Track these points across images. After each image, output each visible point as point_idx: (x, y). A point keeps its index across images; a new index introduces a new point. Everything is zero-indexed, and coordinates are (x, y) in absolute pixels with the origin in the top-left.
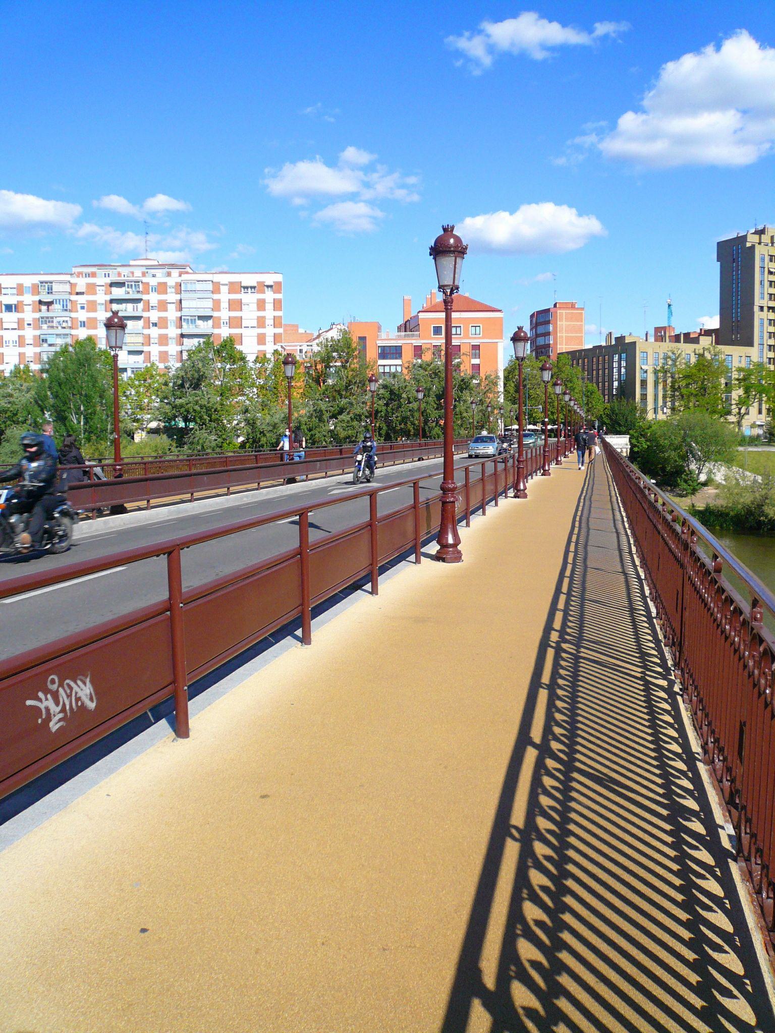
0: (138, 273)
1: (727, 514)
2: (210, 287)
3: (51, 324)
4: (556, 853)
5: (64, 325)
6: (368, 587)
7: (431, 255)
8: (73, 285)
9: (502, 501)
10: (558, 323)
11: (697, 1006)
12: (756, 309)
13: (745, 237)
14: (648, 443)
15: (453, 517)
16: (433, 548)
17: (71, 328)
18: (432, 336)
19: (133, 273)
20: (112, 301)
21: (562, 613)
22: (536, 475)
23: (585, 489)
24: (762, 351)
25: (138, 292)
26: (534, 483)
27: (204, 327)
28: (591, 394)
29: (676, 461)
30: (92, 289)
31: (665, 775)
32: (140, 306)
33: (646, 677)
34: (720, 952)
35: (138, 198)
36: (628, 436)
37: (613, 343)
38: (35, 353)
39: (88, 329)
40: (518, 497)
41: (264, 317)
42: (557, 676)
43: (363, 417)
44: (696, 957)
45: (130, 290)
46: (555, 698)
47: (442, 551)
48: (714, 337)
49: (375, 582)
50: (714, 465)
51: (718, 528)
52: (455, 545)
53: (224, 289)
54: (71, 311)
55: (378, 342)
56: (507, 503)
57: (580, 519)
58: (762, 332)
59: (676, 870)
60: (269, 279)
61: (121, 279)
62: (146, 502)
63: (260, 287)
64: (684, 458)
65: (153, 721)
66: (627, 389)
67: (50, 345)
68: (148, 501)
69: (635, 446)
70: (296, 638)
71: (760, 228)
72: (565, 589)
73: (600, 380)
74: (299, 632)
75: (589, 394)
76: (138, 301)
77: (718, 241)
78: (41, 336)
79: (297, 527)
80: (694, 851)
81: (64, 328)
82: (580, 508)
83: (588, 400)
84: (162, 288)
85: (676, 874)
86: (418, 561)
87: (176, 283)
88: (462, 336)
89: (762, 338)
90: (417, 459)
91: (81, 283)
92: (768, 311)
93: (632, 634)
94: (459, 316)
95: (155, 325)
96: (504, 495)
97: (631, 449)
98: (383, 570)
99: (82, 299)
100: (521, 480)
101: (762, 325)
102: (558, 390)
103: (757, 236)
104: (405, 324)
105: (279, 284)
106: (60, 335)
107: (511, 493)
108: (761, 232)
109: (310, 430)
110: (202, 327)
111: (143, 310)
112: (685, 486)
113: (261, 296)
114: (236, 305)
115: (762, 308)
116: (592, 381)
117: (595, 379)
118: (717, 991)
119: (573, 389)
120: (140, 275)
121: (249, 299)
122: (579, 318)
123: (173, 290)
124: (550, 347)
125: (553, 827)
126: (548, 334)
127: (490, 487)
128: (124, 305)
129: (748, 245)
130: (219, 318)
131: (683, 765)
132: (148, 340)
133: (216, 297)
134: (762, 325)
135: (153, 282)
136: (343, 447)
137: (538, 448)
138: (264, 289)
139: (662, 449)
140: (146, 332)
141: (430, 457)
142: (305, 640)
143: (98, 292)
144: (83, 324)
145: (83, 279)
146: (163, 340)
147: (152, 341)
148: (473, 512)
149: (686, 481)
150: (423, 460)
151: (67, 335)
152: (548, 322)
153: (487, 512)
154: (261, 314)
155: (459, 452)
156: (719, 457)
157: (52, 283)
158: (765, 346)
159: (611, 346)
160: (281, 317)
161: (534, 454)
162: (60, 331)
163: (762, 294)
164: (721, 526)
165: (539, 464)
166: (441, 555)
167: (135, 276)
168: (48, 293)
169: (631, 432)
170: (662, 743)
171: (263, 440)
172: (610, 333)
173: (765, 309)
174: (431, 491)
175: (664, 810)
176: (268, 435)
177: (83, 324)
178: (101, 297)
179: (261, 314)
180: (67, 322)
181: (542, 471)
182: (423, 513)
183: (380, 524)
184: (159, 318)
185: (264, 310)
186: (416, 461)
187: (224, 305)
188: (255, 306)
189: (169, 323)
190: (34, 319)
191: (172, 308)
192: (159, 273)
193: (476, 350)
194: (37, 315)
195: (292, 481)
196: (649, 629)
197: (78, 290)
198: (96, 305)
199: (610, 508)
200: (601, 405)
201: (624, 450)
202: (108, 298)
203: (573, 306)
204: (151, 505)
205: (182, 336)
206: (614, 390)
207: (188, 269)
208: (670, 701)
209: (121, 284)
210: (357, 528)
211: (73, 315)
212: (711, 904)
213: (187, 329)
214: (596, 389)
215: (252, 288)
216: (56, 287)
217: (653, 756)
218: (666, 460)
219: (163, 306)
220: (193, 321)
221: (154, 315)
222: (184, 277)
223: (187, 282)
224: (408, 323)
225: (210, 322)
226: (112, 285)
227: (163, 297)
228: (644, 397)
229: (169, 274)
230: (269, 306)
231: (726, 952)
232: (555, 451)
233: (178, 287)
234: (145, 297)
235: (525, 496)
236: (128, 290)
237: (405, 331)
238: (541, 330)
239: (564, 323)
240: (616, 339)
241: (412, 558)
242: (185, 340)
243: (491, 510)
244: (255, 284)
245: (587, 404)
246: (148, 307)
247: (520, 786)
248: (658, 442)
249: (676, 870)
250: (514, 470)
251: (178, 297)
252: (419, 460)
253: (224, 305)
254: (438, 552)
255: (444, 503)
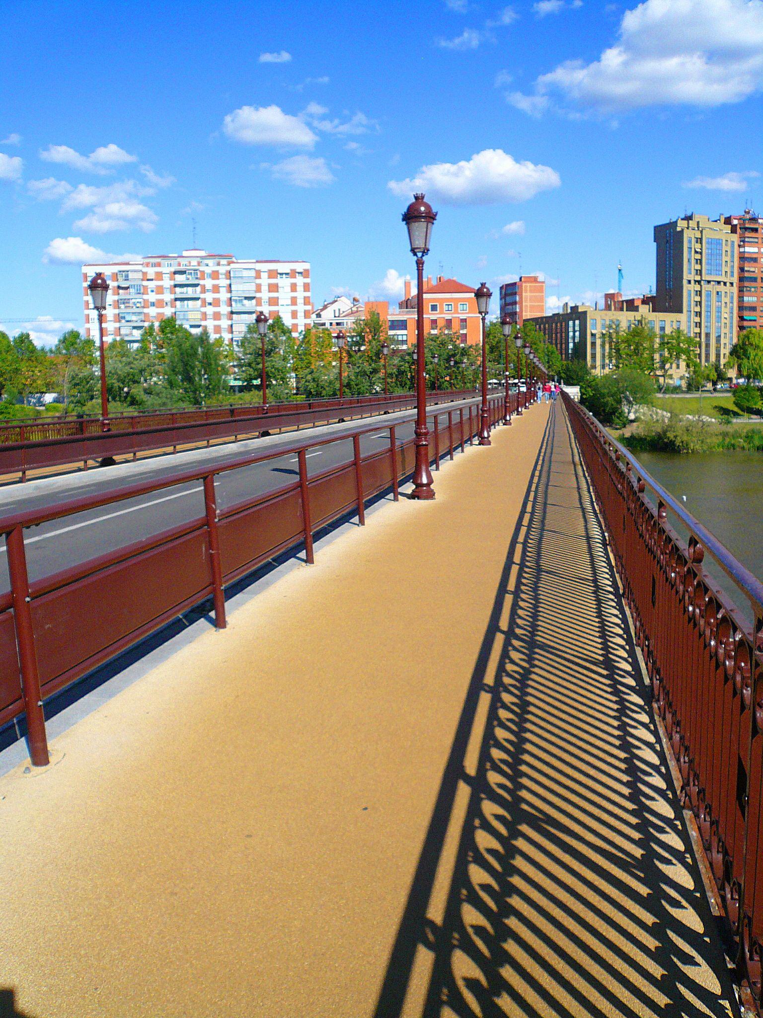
0: (194, 262)
1: (645, 439)
2: (253, 273)
3: (127, 305)
4: (516, 736)
5: (138, 305)
6: (303, 554)
7: (403, 220)
8: (145, 274)
9: (468, 449)
10: (524, 294)
11: (655, 975)
12: (685, 282)
13: (676, 222)
14: (593, 392)
15: (427, 459)
16: (409, 488)
17: (144, 307)
18: (430, 312)
19: (190, 262)
20: (176, 286)
21: (511, 596)
22: (498, 425)
23: (546, 439)
24: (690, 317)
25: (197, 278)
26: (496, 431)
27: (249, 305)
28: (551, 354)
29: (612, 405)
30: (159, 276)
31: (632, 770)
32: (198, 289)
33: (635, 761)
34: (678, 907)
35: (85, 150)
36: (579, 387)
37: (569, 311)
38: (115, 328)
39: (157, 307)
40: (506, 425)
41: (296, 298)
42: (499, 704)
43: (394, 375)
44: (669, 1001)
45: (189, 277)
46: (520, 592)
47: (417, 490)
48: (651, 305)
49: (309, 548)
50: (639, 407)
51: (639, 448)
52: (428, 485)
53: (264, 276)
54: (143, 294)
55: (388, 317)
56: (472, 449)
57: (537, 487)
58: (690, 301)
59: (637, 839)
60: (300, 267)
61: (182, 268)
62: (206, 442)
63: (293, 274)
64: (619, 402)
65: (187, 624)
66: (580, 350)
67: (128, 321)
68: (280, 429)
69: (584, 394)
70: (210, 620)
71: (689, 214)
72: (517, 558)
73: (558, 341)
74: (212, 614)
75: (549, 354)
76: (196, 285)
77: (655, 225)
78: (120, 314)
79: (390, 439)
80: (674, 909)
81: (138, 307)
82: (542, 454)
83: (548, 359)
84: (215, 275)
85: (634, 827)
86: (396, 499)
87: (227, 271)
88: (453, 311)
89: (689, 306)
90: (383, 412)
91: (151, 272)
92: (695, 284)
93: (591, 575)
94: (450, 297)
95: (210, 304)
96: (469, 442)
97: (581, 397)
98: (318, 536)
99: (152, 285)
100: (424, 468)
101: (689, 295)
102: (527, 350)
103: (686, 222)
104: (407, 302)
105: (307, 271)
106: (135, 313)
107: (476, 441)
108: (688, 218)
109: (357, 385)
110: (247, 305)
111: (201, 293)
112: (617, 421)
113: (293, 280)
114: (274, 288)
115: (689, 282)
116: (551, 343)
117: (554, 342)
118: (674, 932)
119: (536, 350)
120: (196, 264)
121: (284, 283)
122: (541, 290)
123: (224, 276)
124: (516, 314)
125: (515, 700)
126: (515, 303)
127: (456, 436)
128: (185, 288)
129: (679, 229)
130: (261, 299)
131: (668, 807)
132: (204, 316)
133: (258, 281)
134: (689, 295)
135: (208, 270)
136: (311, 401)
137: (496, 401)
138: (296, 276)
139: (603, 396)
140: (203, 310)
141: (396, 410)
142: (219, 623)
143: (164, 278)
144: (153, 304)
145: (151, 268)
146: (217, 316)
147: (208, 317)
148: (443, 457)
149: (618, 418)
150: (389, 413)
151: (141, 313)
152: (515, 294)
153: (454, 458)
154: (294, 294)
155: (381, 413)
156: (642, 401)
157: (128, 271)
158: (692, 312)
159: (567, 314)
160: (309, 297)
161: (496, 405)
162: (135, 310)
163: (690, 270)
164: (641, 447)
165: (500, 415)
166: (415, 494)
167: (192, 264)
168: (125, 280)
169: (581, 384)
170: (643, 799)
171: (324, 393)
172: (567, 303)
173: (692, 282)
174: (406, 434)
175: (651, 939)
176: (327, 389)
177: (153, 304)
178: (167, 283)
179: (294, 294)
180: (140, 303)
181: (504, 421)
182: (398, 458)
183: (38, 601)
184: (214, 299)
185: (296, 291)
186: (382, 415)
187: (265, 288)
188: (289, 289)
189: (221, 303)
190: (114, 301)
191: (223, 290)
192: (210, 262)
193: (463, 322)
194: (116, 298)
195: (266, 434)
196: (623, 638)
197: (149, 277)
198: (163, 289)
199: (575, 485)
200: (559, 363)
201: (576, 397)
202: (172, 283)
203: (535, 280)
204: (27, 478)
205: (232, 313)
206: (570, 350)
207: (234, 259)
208: (618, 607)
209: (182, 272)
210: (337, 469)
211: (145, 297)
212: (670, 857)
213: (236, 307)
214: (555, 349)
215: (286, 274)
216: (131, 276)
217: (625, 781)
218: (606, 404)
219: (216, 289)
220: (241, 301)
221: (209, 297)
222: (232, 265)
223: (235, 270)
224: (409, 302)
225: (254, 301)
226: (175, 273)
227: (216, 282)
228: (594, 356)
229: (219, 264)
230: (300, 288)
231: (683, 907)
232: (516, 401)
233: (228, 275)
234: (201, 282)
235: (510, 424)
236: (188, 276)
237: (407, 308)
238: (509, 299)
239: (529, 294)
240: (572, 308)
241: (391, 496)
242: (234, 316)
243: (458, 456)
244: (288, 271)
245: (548, 362)
246: (204, 290)
247: (479, 712)
248: (599, 391)
249: (634, 824)
250: (478, 419)
251: (228, 282)
252: (385, 413)
253: (265, 288)
254: (413, 491)
255: (418, 447)
